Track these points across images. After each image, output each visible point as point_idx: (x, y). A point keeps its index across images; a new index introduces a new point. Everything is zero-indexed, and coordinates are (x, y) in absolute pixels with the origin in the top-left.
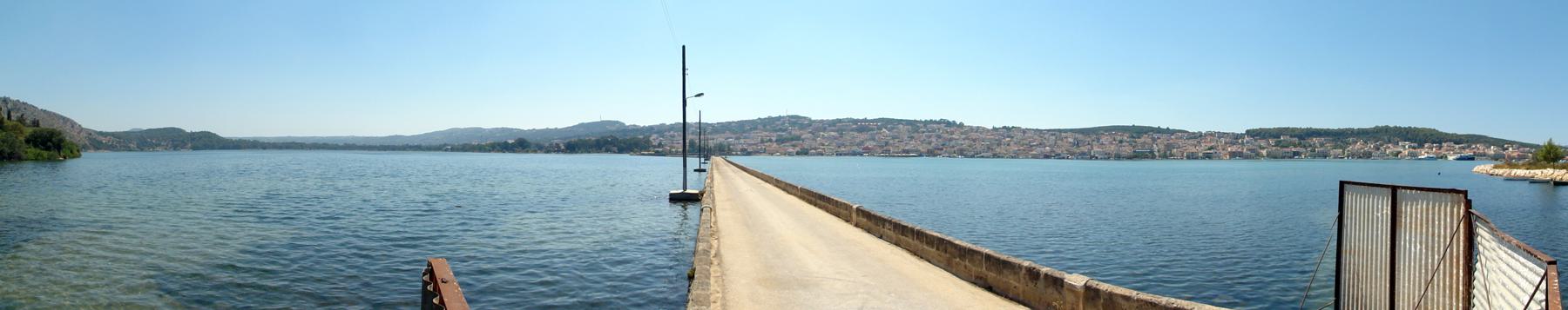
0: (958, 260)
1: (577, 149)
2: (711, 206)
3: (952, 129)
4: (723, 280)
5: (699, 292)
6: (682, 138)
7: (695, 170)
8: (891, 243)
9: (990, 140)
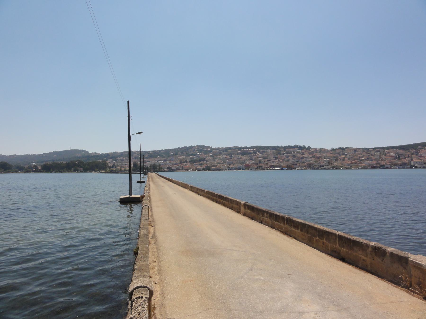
0: (317, 238)
1: (51, 170)
2: (148, 205)
3: (303, 151)
4: (158, 254)
5: (141, 263)
6: (128, 161)
7: (138, 182)
8: (268, 226)
9: (329, 157)
